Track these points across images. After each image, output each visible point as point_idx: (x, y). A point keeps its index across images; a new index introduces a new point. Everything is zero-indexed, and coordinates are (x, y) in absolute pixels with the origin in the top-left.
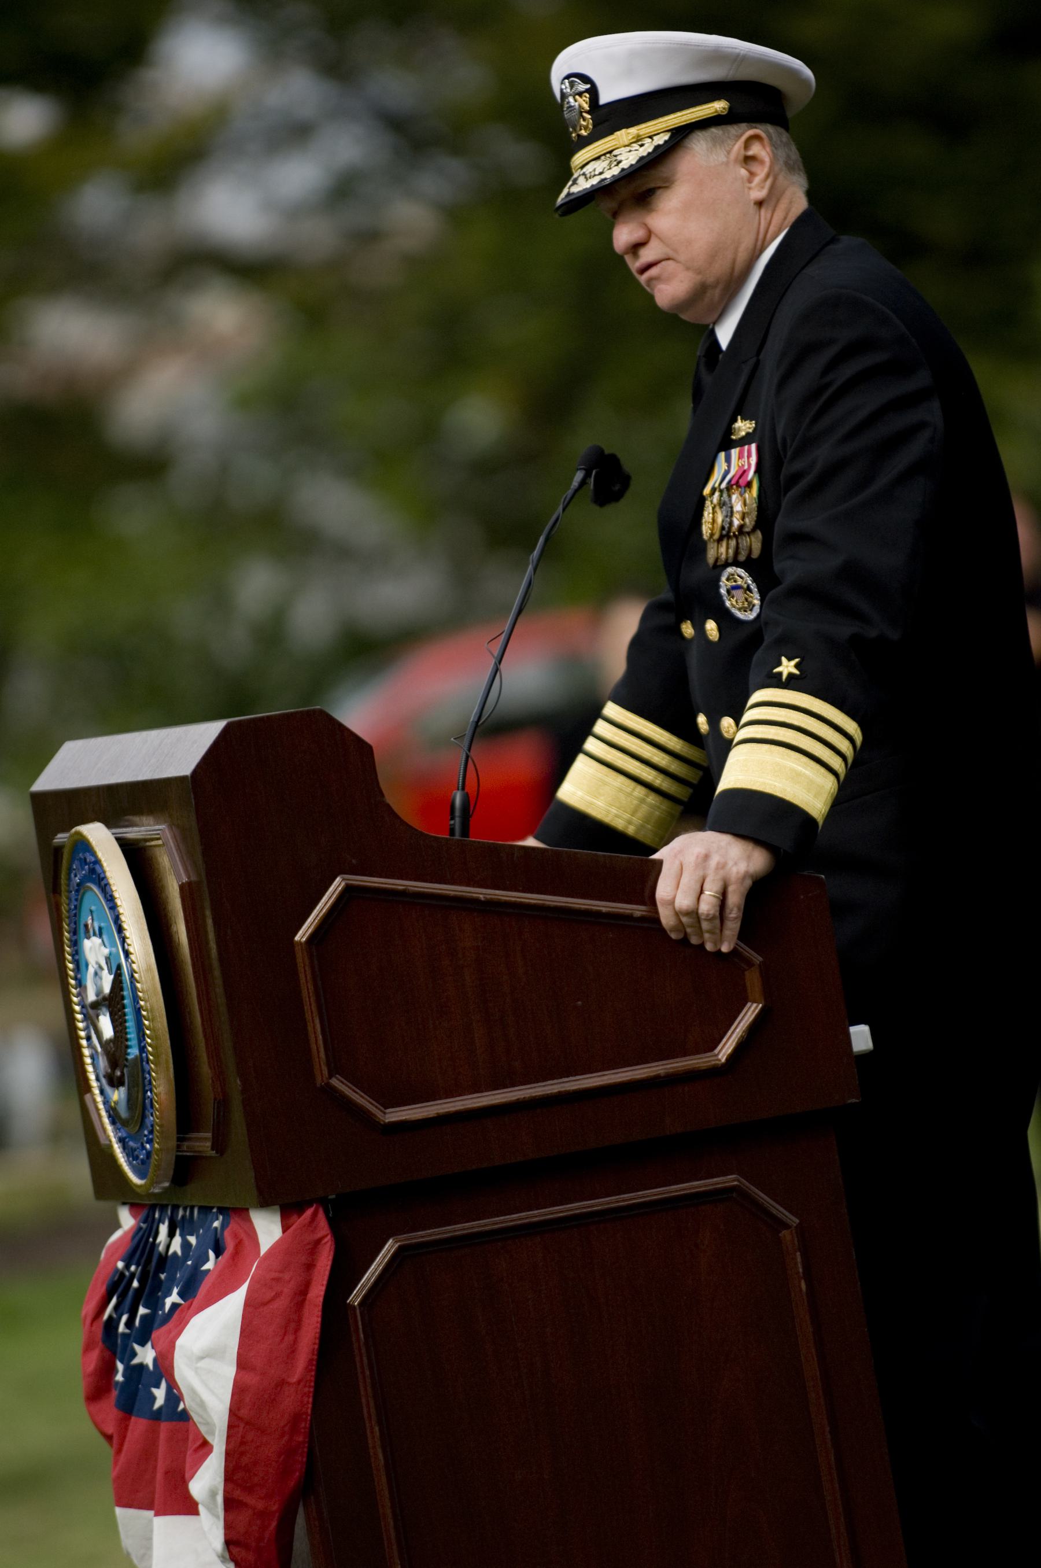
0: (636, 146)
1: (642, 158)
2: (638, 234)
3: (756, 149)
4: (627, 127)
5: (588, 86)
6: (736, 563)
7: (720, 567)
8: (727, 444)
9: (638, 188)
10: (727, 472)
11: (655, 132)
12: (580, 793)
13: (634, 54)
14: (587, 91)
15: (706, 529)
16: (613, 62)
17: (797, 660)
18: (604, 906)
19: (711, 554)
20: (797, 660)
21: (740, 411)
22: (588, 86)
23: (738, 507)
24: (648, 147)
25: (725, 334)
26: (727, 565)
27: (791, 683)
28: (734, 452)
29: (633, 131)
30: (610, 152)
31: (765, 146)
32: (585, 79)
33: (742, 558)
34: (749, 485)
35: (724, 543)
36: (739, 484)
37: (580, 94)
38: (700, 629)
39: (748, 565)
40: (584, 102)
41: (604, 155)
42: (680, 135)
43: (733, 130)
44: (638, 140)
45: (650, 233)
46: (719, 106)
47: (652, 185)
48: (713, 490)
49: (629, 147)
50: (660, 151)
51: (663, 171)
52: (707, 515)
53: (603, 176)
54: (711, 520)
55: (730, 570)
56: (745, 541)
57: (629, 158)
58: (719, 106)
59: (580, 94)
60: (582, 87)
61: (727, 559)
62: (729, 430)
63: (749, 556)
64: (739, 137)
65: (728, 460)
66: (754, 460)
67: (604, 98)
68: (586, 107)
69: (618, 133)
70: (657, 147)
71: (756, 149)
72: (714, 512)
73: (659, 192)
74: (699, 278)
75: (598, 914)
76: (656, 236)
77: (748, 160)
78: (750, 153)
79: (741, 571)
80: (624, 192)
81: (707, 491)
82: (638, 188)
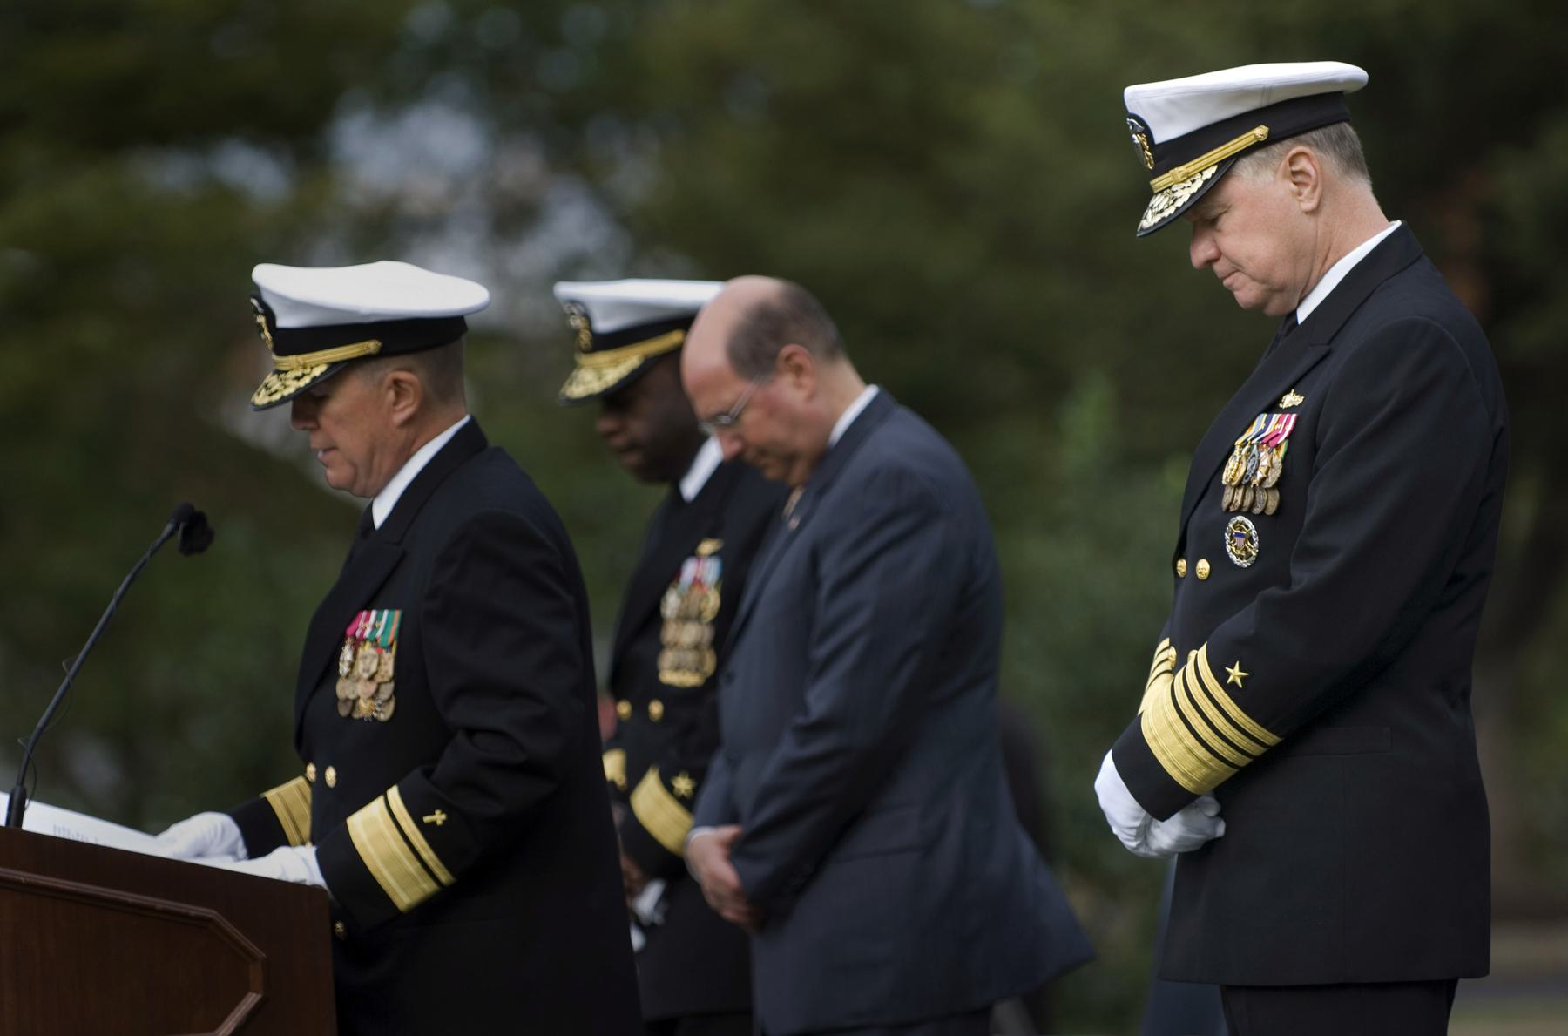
0: (1189, 183)
1: (1193, 195)
3: (1303, 164)
6: (1249, 514)
7: (1229, 514)
8: (1273, 408)
10: (1263, 431)
11: (1203, 169)
15: (1227, 475)
16: (1163, 104)
19: (1227, 499)
21: (1294, 386)
23: (1265, 462)
25: (381, 511)
26: (1239, 512)
28: (1276, 417)
31: (1315, 156)
33: (1257, 511)
34: (1278, 447)
35: (1241, 491)
36: (1269, 442)
38: (1192, 566)
39: (1258, 519)
43: (1276, 149)
44: (1189, 177)
46: (1261, 132)
48: (1245, 442)
50: (1209, 186)
52: (1232, 463)
54: (1233, 469)
55: (1240, 518)
56: (1261, 497)
57: (1184, 195)
58: (1261, 132)
61: (1241, 506)
62: (1279, 400)
63: (1263, 513)
65: (1268, 422)
66: (1289, 428)
67: (1159, 138)
70: (1206, 182)
71: (1303, 164)
72: (1240, 462)
79: (1250, 524)
81: (1239, 441)
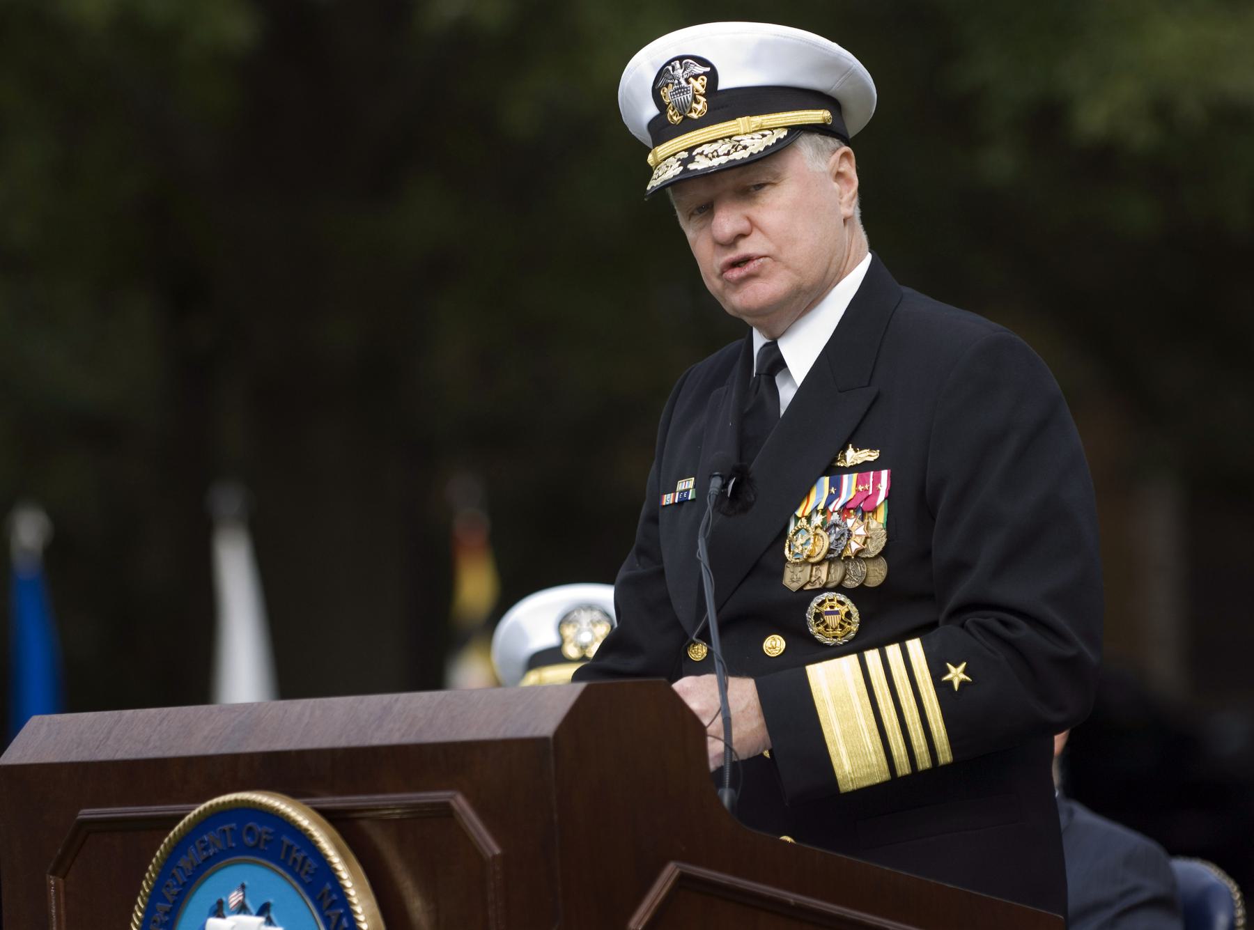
2: (743, 226)
4: (751, 115)
5: (708, 69)
9: (747, 178)
12: (847, 767)
13: (763, 44)
14: (705, 74)
17: (964, 665)
18: (792, 897)
20: (964, 665)
22: (708, 69)
24: (771, 140)
27: (942, 688)
29: (757, 120)
30: (730, 137)
32: (702, 62)
37: (696, 77)
40: (699, 85)
41: (722, 139)
42: (795, 131)
45: (753, 224)
47: (763, 180)
49: (751, 135)
51: (775, 166)
53: (731, 157)
57: (756, 145)
58: (819, 116)
59: (696, 77)
60: (700, 69)
64: (834, 151)
68: (702, 91)
69: (739, 119)
73: (767, 188)
74: (797, 278)
75: (784, 904)
76: (760, 230)
77: (839, 175)
78: (842, 169)
80: (730, 181)
82: (747, 178)
